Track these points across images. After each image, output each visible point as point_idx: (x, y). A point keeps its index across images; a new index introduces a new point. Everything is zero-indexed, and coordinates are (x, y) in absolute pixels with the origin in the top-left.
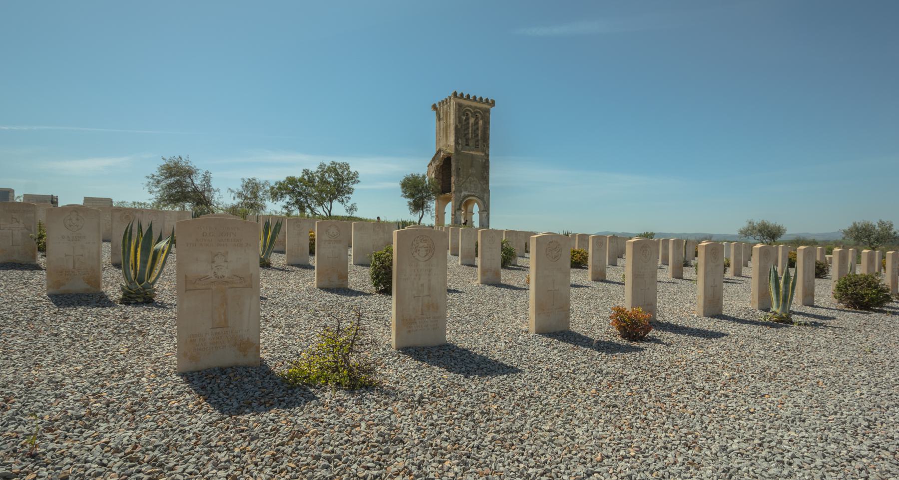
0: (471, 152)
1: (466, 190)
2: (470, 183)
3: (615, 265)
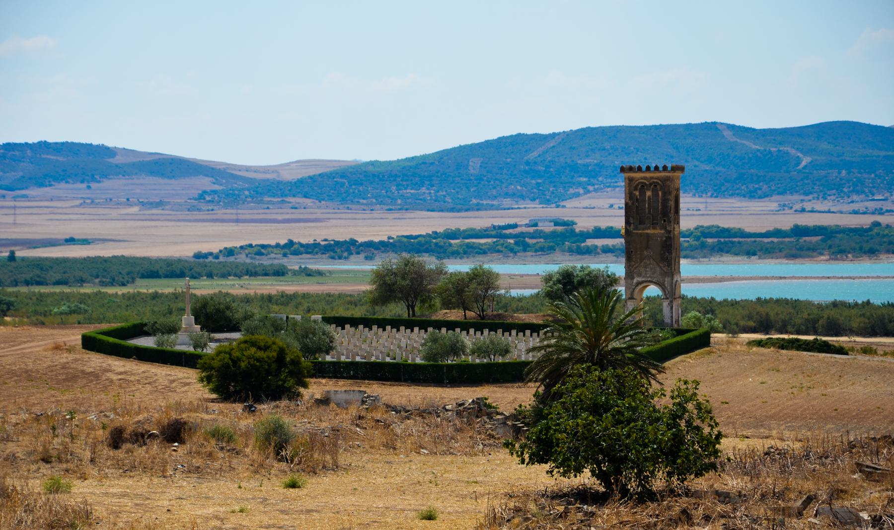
0: (646, 231)
1: (639, 275)
2: (646, 267)
3: (890, 436)
